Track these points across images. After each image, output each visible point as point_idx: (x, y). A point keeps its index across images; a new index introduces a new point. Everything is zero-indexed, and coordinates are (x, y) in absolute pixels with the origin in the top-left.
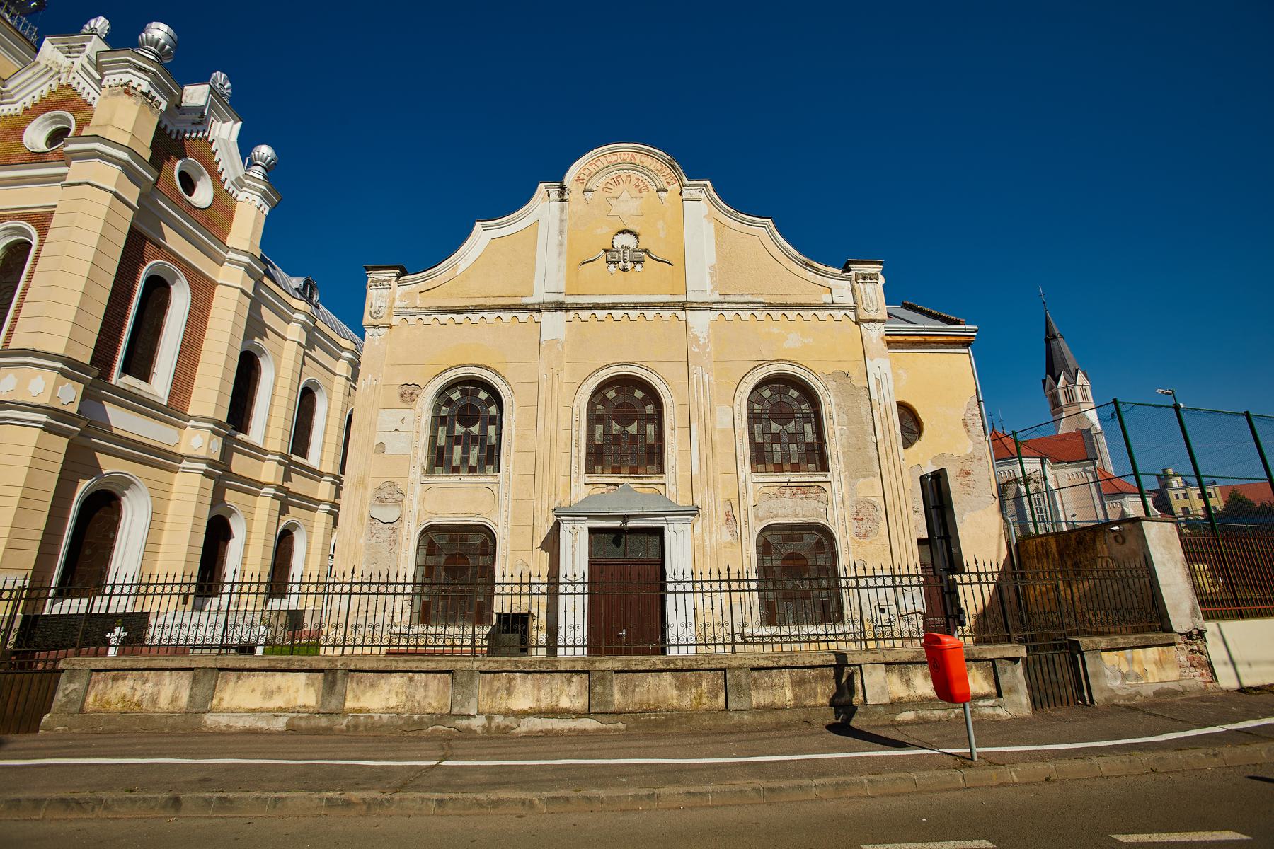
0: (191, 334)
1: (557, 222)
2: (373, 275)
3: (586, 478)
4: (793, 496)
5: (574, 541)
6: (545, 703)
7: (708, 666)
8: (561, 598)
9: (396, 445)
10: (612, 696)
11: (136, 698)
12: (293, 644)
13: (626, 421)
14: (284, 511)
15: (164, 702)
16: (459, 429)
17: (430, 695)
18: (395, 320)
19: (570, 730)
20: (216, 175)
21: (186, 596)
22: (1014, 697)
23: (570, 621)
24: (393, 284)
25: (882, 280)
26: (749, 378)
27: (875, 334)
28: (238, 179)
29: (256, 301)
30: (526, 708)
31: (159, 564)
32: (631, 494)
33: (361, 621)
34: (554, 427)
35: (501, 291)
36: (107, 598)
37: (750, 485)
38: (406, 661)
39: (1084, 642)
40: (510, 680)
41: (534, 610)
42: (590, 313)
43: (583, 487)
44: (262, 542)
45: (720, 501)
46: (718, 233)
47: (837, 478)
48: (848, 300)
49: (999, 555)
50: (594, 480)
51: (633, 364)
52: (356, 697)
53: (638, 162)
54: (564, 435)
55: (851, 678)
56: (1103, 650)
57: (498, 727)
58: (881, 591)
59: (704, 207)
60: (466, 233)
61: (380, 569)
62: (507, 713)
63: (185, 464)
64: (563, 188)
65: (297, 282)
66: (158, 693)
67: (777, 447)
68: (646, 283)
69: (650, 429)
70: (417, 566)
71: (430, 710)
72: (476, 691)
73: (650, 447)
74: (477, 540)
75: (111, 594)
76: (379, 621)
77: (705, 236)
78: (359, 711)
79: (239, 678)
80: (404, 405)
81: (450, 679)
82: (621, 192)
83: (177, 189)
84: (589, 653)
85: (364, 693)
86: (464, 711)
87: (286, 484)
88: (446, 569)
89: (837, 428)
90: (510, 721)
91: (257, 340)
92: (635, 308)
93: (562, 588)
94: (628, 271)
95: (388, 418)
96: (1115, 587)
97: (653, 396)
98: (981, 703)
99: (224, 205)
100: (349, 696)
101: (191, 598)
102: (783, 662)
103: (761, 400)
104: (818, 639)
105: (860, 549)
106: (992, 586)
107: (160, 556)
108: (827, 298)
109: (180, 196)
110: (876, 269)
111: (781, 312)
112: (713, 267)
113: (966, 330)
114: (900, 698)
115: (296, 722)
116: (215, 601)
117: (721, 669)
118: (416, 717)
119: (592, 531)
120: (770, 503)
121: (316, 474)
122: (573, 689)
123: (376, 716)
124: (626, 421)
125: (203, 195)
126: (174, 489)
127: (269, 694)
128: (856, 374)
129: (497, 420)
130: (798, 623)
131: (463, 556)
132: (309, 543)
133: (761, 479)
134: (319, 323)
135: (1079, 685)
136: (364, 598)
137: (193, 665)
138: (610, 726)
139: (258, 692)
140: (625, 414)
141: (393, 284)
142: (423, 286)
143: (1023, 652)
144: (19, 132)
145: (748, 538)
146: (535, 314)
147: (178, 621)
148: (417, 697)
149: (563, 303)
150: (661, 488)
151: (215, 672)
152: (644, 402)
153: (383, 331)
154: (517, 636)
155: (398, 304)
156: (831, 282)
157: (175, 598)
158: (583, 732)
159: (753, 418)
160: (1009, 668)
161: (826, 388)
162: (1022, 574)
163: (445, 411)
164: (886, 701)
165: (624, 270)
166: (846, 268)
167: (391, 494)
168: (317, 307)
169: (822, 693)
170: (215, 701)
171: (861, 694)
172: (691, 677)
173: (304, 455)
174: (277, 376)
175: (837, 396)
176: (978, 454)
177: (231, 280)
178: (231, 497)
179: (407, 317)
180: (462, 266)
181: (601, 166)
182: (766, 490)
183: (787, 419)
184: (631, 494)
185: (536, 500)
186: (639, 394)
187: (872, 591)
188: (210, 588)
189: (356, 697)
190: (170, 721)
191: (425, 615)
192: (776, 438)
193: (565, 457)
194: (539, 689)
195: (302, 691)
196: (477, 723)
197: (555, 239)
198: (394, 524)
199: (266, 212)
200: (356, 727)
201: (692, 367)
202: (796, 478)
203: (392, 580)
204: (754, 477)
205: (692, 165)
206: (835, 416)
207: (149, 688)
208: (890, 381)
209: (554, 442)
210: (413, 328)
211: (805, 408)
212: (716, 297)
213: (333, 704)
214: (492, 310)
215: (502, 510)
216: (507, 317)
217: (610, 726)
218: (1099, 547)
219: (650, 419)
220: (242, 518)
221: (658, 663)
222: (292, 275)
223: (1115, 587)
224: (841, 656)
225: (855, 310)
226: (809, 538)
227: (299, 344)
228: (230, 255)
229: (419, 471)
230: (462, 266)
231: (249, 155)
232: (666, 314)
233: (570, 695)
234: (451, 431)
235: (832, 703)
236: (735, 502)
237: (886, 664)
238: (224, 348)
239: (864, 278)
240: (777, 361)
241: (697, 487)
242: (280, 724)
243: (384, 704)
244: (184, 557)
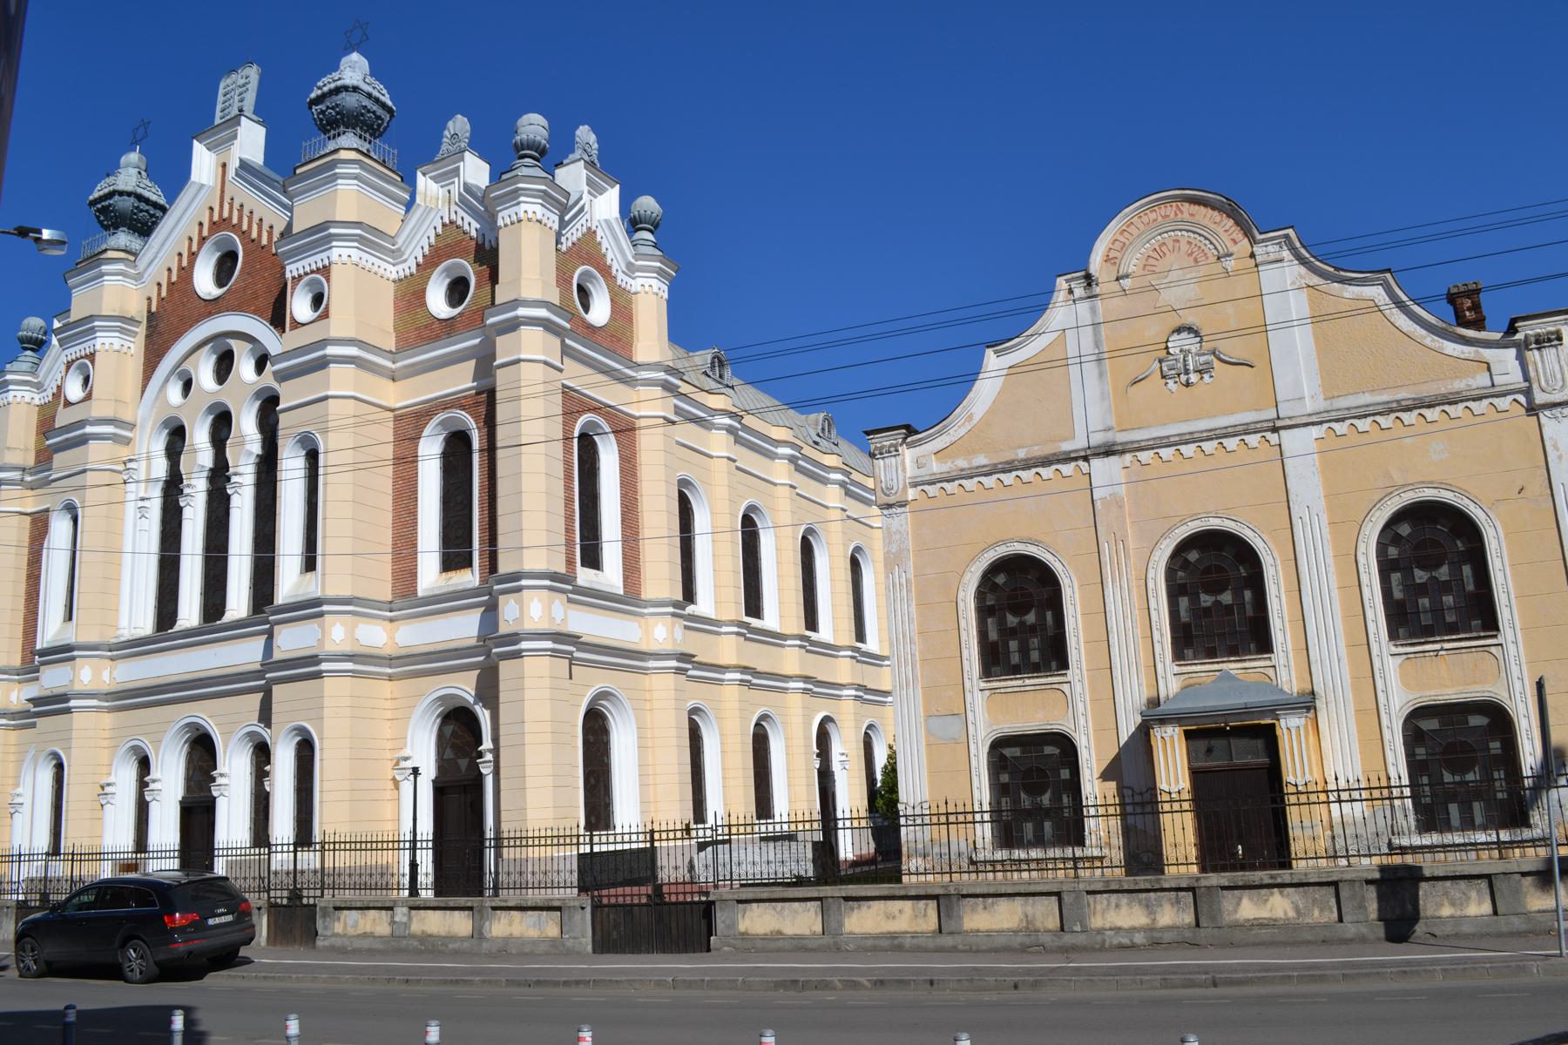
13: (1218, 592)
16: (1012, 620)
18: (911, 494)
32: (1227, 682)
42: (1151, 453)
43: (1172, 680)
48: (1514, 377)
59: (1292, 272)
64: (1089, 279)
67: (1425, 602)
68: (1221, 401)
77: (1297, 321)
124: (1218, 592)
125: (600, 312)
144: (420, 295)
147: (765, 858)
150: (1271, 672)
156: (1488, 354)
165: (1188, 384)
166: (1512, 329)
183: (1435, 569)
184: (1227, 682)
192: (1422, 590)
212: (1321, 405)
214: (1027, 465)
234: (1002, 623)
239: (1537, 342)
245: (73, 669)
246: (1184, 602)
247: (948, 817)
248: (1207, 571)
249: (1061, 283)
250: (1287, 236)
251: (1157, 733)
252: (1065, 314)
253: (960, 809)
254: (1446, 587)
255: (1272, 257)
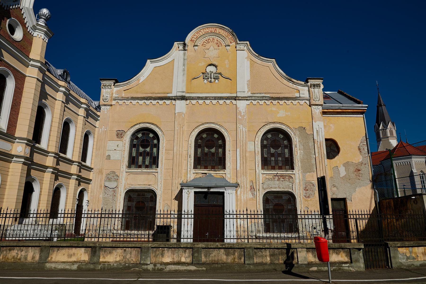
0: (16, 100)
1: (182, 60)
2: (103, 83)
3: (193, 171)
4: (279, 179)
5: (188, 197)
6: (176, 260)
7: (237, 247)
8: (183, 220)
9: (115, 156)
10: (201, 257)
11: (19, 257)
12: (74, 238)
13: (210, 148)
14: (56, 179)
15: (29, 259)
16: (141, 149)
17: (132, 256)
18: (114, 102)
19: (185, 270)
20: (24, 25)
21: (16, 218)
22: (358, 264)
23: (186, 229)
24: (112, 86)
25: (322, 87)
26: (262, 130)
27: (317, 110)
28: (34, 26)
29: (43, 83)
30: (169, 261)
31: (4, 204)
33: (105, 228)
34: (181, 149)
35: (158, 91)
36: (4, 219)
37: (261, 175)
38: (123, 243)
39: (390, 243)
40: (163, 251)
41: (172, 224)
43: (192, 174)
44: (47, 193)
45: (248, 181)
46: (252, 66)
47: (297, 172)
48: (307, 95)
49: (370, 207)
50: (197, 171)
51: (213, 123)
52: (104, 257)
53: (217, 32)
54: (185, 153)
55: (293, 253)
56: (399, 247)
57: (158, 269)
58: (314, 220)
60: (142, 65)
61: (108, 208)
62: (162, 264)
63: (15, 159)
64: (185, 45)
65: (59, 72)
66: (27, 255)
67: (273, 159)
68: (220, 88)
69: (220, 150)
70: (124, 206)
71: (132, 262)
72: (150, 255)
73: (220, 158)
74: (149, 195)
75: (6, 217)
76: (91, 228)
77: (246, 66)
78: (105, 262)
79: (58, 250)
80: (118, 139)
81: (140, 250)
82: (210, 47)
83: (7, 33)
84: (193, 241)
85: (107, 256)
86: (145, 262)
87: (58, 167)
88: (136, 207)
89: (299, 151)
90: (163, 267)
91: (43, 101)
92: (215, 99)
93: (183, 216)
94: (213, 82)
95: (112, 145)
96: (413, 222)
97: (222, 137)
98: (343, 265)
99: (28, 39)
100: (101, 257)
101: (18, 219)
102: (266, 246)
103: (267, 139)
104: (277, 238)
105: (306, 202)
106: (367, 221)
107: (5, 200)
108: (297, 95)
109: (9, 36)
110: (320, 82)
111: (277, 101)
112: (249, 81)
113: (362, 107)
114: (312, 262)
115: (81, 266)
116: (27, 220)
117: (243, 248)
118: (127, 265)
119: (195, 192)
120: (269, 182)
121: (70, 162)
122: (187, 254)
123: (112, 264)
124: (210, 148)
125: (18, 35)
126: (10, 170)
127: (70, 256)
128: (308, 128)
129: (157, 146)
130: (281, 232)
131: (143, 202)
132: (67, 193)
133: (265, 172)
134: (71, 92)
135: (387, 260)
136: (106, 219)
137: (41, 245)
138: (200, 269)
139: (66, 256)
140: (210, 143)
141: (112, 86)
142: (125, 87)
143: (363, 247)
145: (259, 197)
146: (173, 101)
148: (127, 257)
149: (185, 96)
150: (224, 175)
151: (49, 247)
152: (218, 139)
153: (108, 107)
154: (165, 235)
155: (114, 95)
156: (300, 88)
157: (11, 219)
158: (190, 271)
159: (263, 147)
160: (356, 253)
161: (295, 134)
162: (381, 215)
163: (135, 142)
164: (306, 263)
165: (211, 82)
167: (113, 176)
168: (69, 83)
169: (281, 259)
170: (49, 259)
171: (296, 260)
172: (231, 251)
173: (65, 153)
174: (53, 117)
175: (299, 138)
176: (364, 162)
177: (32, 74)
178: (34, 173)
179: (119, 101)
180: (142, 79)
181: (201, 34)
182: (267, 177)
183: (277, 148)
185: (172, 179)
186: (216, 136)
187: (310, 220)
188: (24, 215)
189: (104, 257)
190: (33, 266)
191: (127, 226)
192: (272, 155)
193: (185, 162)
194: (174, 254)
195: (83, 255)
196: (150, 267)
197: (181, 68)
198: (115, 190)
199: (47, 41)
200: (104, 268)
201: (238, 125)
202: (280, 172)
203: (114, 212)
204: (262, 172)
205: (241, 35)
206: (298, 146)
207: (23, 253)
208: (323, 131)
209: (180, 156)
210: (121, 106)
211: (286, 142)
212: (249, 94)
213: (95, 259)
214: (155, 99)
215: (159, 183)
216: (161, 102)
217: (200, 269)
218: (408, 205)
219: (220, 146)
220: (38, 182)
221: (219, 245)
222: (58, 68)
223: (413, 222)
224: (289, 245)
225: (309, 100)
226: (285, 197)
227: (62, 102)
228: (32, 62)
229: (125, 167)
230: (142, 79)
231: (38, 13)
232: (228, 102)
233: (185, 257)
235: (285, 263)
236: (254, 181)
237: (307, 248)
238: (30, 106)
239: (314, 86)
240: (274, 123)
241: (239, 175)
242: (75, 267)
243: (115, 260)
244: (15, 200)
245: (12, 146)
246: (199, 150)
247: (104, 215)
248: (208, 141)
249: (176, 43)
250: (247, 44)
251: (185, 192)
252: (176, 52)
253: (253, 213)
254: (279, 155)
255: (242, 49)
